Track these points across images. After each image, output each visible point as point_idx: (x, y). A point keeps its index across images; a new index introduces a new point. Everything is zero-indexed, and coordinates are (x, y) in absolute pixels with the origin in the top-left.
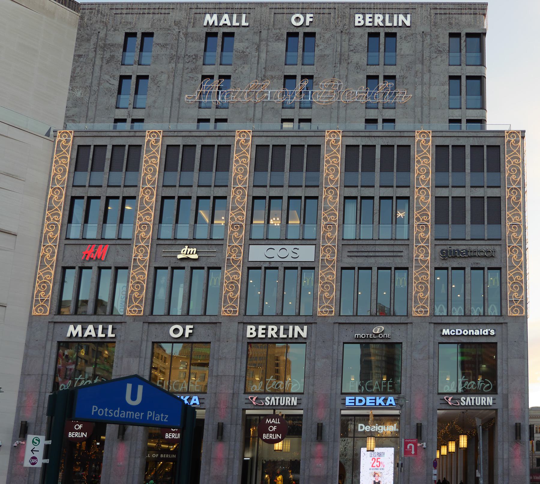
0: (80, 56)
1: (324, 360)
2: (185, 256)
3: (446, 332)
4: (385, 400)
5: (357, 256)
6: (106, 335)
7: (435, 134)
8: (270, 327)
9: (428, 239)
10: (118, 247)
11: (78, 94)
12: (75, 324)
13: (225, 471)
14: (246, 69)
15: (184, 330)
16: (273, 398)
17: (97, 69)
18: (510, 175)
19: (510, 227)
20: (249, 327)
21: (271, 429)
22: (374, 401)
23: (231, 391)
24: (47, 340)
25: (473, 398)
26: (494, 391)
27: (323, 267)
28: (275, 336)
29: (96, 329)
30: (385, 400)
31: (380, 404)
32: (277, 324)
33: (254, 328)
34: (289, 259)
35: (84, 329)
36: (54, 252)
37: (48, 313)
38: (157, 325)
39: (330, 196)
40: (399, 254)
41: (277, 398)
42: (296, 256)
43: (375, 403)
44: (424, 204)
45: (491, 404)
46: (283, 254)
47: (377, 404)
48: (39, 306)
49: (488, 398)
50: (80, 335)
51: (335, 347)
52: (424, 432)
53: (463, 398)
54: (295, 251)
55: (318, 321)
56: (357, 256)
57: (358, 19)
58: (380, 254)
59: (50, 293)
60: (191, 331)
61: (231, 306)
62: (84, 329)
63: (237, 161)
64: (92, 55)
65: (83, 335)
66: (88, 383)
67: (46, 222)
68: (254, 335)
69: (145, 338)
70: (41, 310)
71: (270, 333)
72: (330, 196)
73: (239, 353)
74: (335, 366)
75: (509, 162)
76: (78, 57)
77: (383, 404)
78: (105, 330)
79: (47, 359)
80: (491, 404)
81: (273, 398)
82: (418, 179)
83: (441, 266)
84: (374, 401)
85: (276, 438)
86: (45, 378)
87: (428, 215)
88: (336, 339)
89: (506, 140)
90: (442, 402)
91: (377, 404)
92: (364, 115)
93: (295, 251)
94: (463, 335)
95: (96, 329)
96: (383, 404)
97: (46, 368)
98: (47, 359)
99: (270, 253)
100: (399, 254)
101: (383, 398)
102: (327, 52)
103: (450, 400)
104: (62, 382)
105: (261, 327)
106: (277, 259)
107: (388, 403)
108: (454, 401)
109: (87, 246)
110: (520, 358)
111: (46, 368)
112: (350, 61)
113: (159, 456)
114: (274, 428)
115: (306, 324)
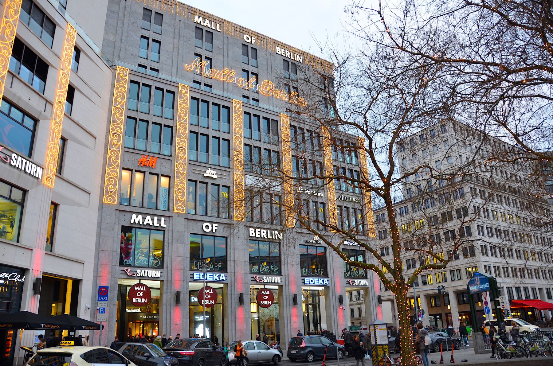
2: (209, 175)
4: (219, 276)
6: (160, 225)
7: (131, 72)
8: (263, 231)
9: (119, 146)
10: (162, 160)
12: (138, 213)
13: (245, 326)
15: (212, 226)
16: (143, 271)
18: (180, 113)
19: (179, 149)
20: (251, 229)
21: (139, 294)
24: (115, 223)
25: (146, 271)
26: (280, 274)
27: (178, 177)
28: (266, 237)
29: (153, 220)
30: (219, 276)
31: (216, 279)
32: (267, 229)
33: (253, 230)
35: (144, 219)
36: (118, 156)
37: (116, 203)
38: (193, 221)
39: (118, 114)
41: (146, 271)
44: (119, 119)
45: (159, 276)
48: (109, 196)
49: (157, 272)
50: (141, 223)
52: (237, 300)
53: (139, 271)
55: (175, 216)
57: (278, 50)
59: (117, 187)
60: (216, 228)
61: (180, 206)
62: (144, 219)
63: (180, 104)
65: (143, 223)
67: (111, 132)
68: (254, 235)
70: (110, 199)
71: (264, 235)
72: (182, 128)
75: (180, 104)
77: (218, 279)
78: (159, 221)
80: (159, 276)
81: (143, 271)
82: (115, 100)
83: (203, 181)
85: (211, 303)
87: (121, 128)
89: (234, 105)
90: (252, 279)
95: (153, 220)
96: (218, 279)
101: (218, 275)
103: (128, 271)
104: (126, 258)
105: (257, 230)
107: (221, 278)
108: (132, 273)
109: (140, 156)
113: (148, 317)
114: (141, 294)
115: (269, 229)
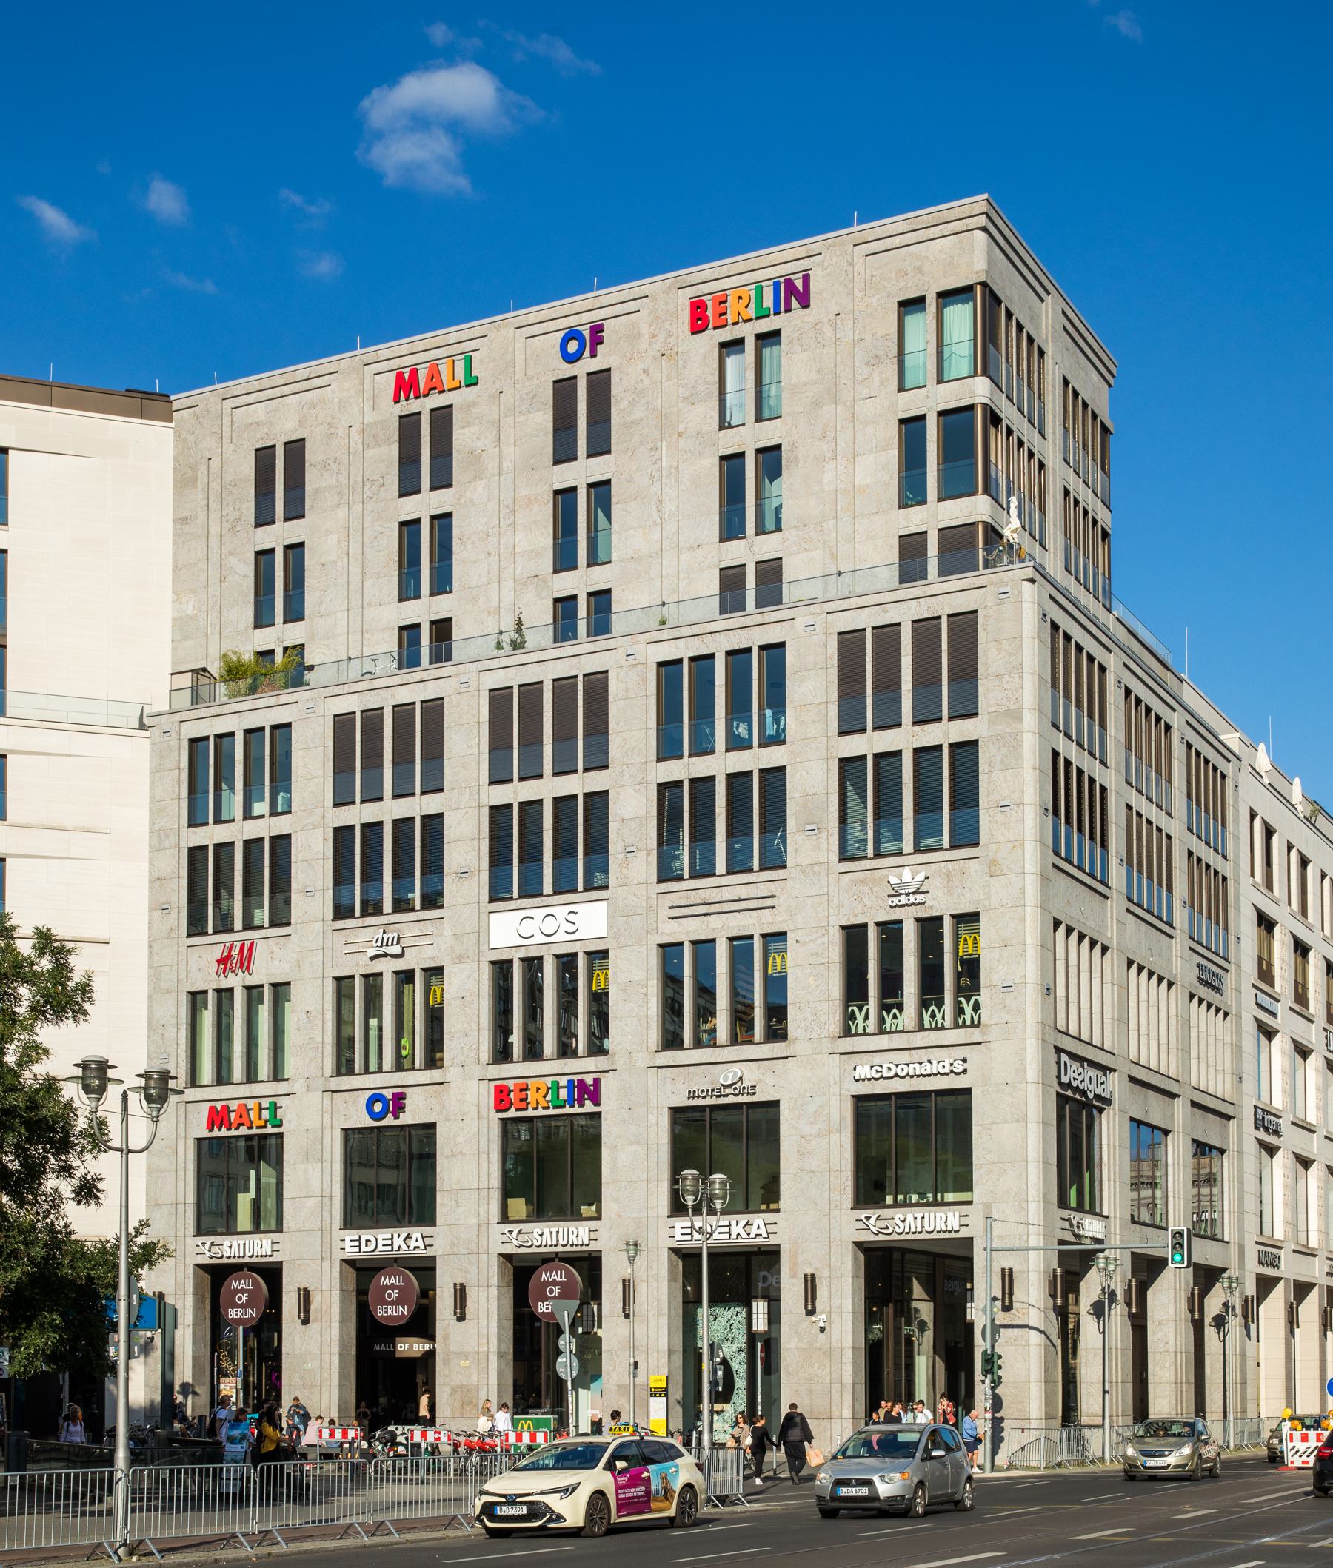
0: (185, 520)
1: (633, 1148)
3: (863, 1071)
5: (740, 900)
11: (189, 609)
13: (474, 1378)
14: (480, 490)
17: (214, 542)
22: (726, 1229)
23: (475, 1221)
34: (561, 936)
40: (769, 902)
42: (571, 928)
43: (729, 1233)
46: (549, 926)
47: (734, 1236)
51: (652, 1119)
54: (571, 917)
56: (740, 900)
58: (726, 907)
64: (202, 515)
66: (247, 1190)
69: (327, 1121)
73: (484, 1141)
74: (653, 1158)
76: (182, 521)
79: (181, 1173)
84: (726, 1229)
86: (181, 1208)
88: (653, 1103)
91: (734, 1236)
92: (716, 560)
93: (571, 917)
94: (896, 1075)
97: (181, 1191)
98: (181, 1173)
99: (527, 928)
100: (769, 902)
102: (637, 415)
106: (540, 939)
110: (1018, 1121)
111: (181, 1191)
112: (682, 427)
